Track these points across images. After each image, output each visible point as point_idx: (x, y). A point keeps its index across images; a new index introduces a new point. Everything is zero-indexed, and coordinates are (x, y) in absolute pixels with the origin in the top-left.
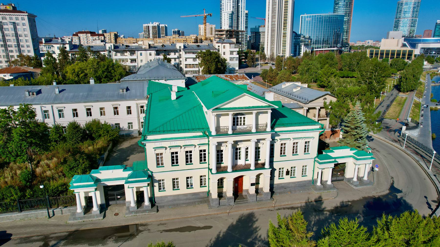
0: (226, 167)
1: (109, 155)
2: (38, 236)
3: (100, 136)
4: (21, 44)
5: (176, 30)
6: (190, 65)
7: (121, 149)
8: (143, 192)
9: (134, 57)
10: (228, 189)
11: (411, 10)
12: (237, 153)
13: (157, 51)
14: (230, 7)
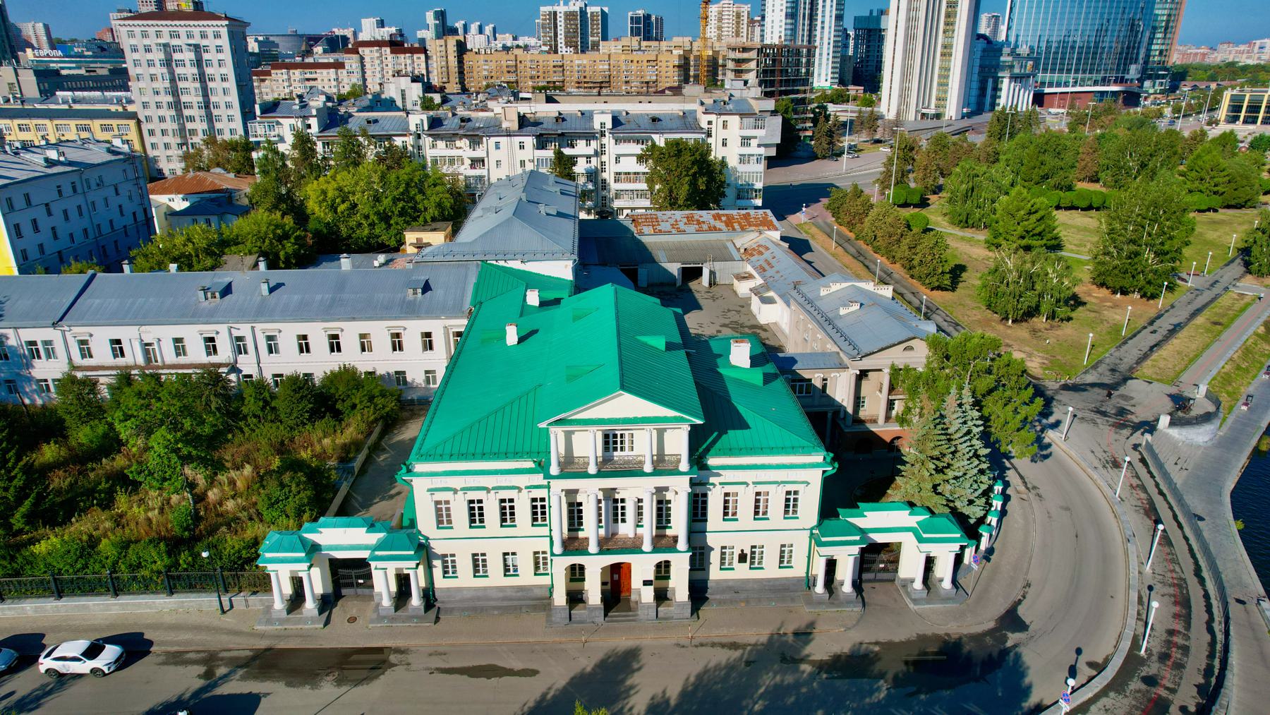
1: (368, 460)
2: (198, 652)
3: (354, 407)
4: (213, 99)
5: (641, 12)
6: (629, 173)
7: (399, 441)
8: (408, 575)
10: (593, 590)
13: (539, 137)
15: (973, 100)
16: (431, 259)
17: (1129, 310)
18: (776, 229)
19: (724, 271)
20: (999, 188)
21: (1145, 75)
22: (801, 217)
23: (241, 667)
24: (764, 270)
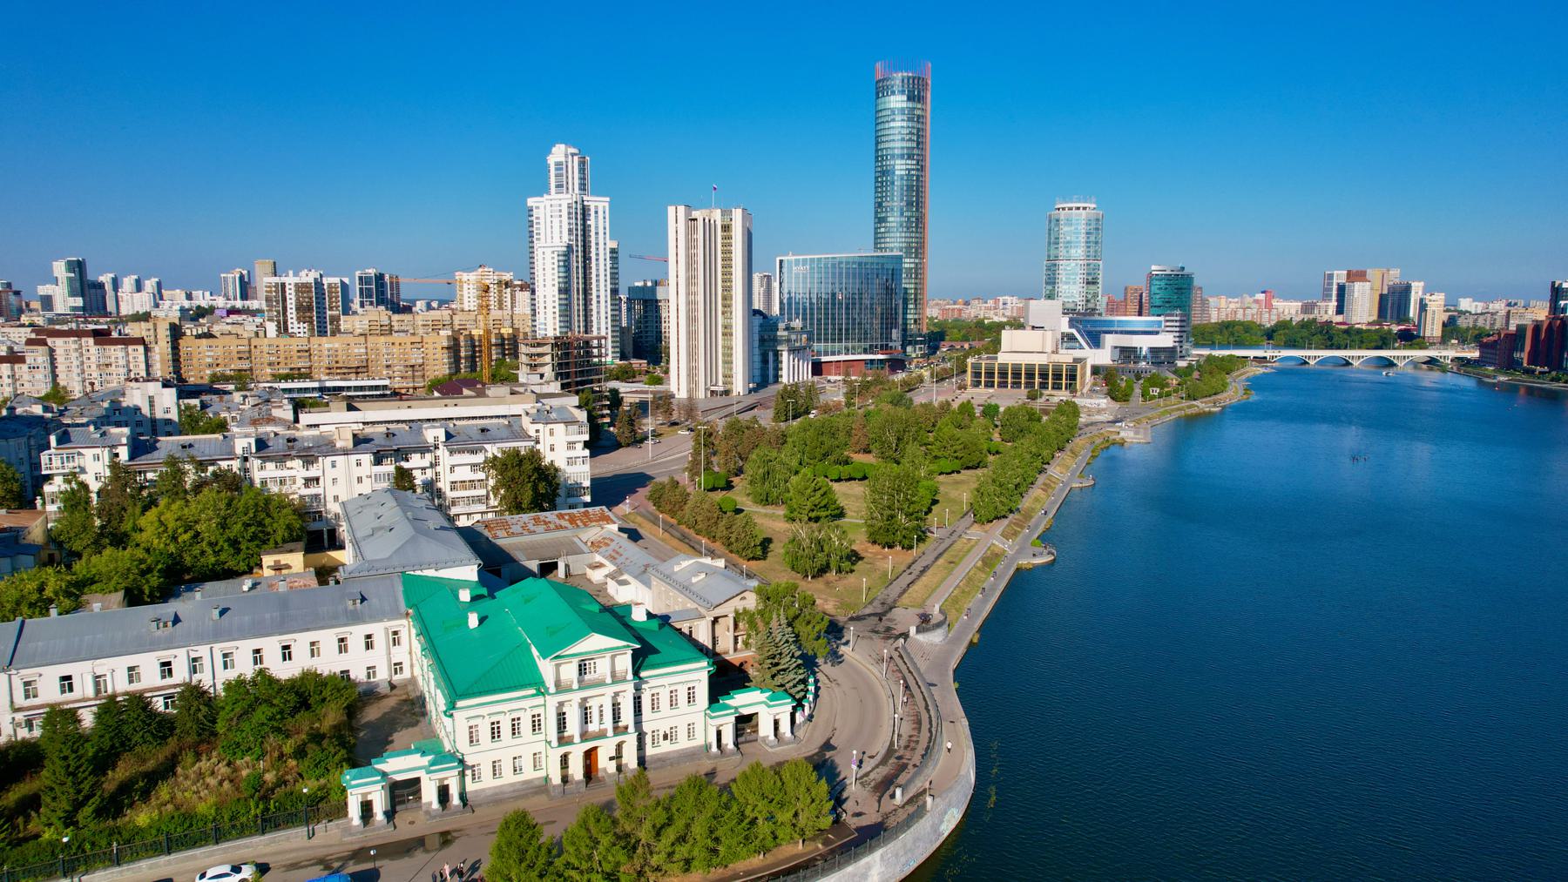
0: (572, 737)
5: (372, 272)
9: (313, 472)
10: (577, 770)
11: (1082, 238)
12: (586, 714)
14: (561, 232)
15: (757, 373)
16: (357, 575)
17: (890, 560)
18: (615, 523)
19: (578, 564)
20: (790, 470)
21: (907, 340)
22: (625, 507)
23: (350, 859)
24: (615, 559)
